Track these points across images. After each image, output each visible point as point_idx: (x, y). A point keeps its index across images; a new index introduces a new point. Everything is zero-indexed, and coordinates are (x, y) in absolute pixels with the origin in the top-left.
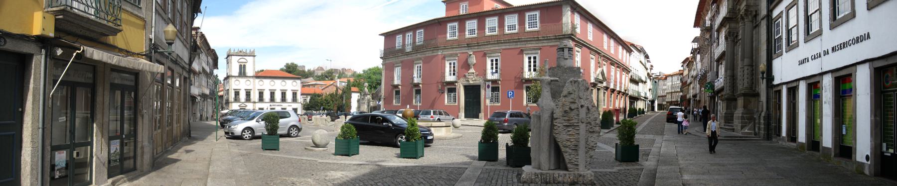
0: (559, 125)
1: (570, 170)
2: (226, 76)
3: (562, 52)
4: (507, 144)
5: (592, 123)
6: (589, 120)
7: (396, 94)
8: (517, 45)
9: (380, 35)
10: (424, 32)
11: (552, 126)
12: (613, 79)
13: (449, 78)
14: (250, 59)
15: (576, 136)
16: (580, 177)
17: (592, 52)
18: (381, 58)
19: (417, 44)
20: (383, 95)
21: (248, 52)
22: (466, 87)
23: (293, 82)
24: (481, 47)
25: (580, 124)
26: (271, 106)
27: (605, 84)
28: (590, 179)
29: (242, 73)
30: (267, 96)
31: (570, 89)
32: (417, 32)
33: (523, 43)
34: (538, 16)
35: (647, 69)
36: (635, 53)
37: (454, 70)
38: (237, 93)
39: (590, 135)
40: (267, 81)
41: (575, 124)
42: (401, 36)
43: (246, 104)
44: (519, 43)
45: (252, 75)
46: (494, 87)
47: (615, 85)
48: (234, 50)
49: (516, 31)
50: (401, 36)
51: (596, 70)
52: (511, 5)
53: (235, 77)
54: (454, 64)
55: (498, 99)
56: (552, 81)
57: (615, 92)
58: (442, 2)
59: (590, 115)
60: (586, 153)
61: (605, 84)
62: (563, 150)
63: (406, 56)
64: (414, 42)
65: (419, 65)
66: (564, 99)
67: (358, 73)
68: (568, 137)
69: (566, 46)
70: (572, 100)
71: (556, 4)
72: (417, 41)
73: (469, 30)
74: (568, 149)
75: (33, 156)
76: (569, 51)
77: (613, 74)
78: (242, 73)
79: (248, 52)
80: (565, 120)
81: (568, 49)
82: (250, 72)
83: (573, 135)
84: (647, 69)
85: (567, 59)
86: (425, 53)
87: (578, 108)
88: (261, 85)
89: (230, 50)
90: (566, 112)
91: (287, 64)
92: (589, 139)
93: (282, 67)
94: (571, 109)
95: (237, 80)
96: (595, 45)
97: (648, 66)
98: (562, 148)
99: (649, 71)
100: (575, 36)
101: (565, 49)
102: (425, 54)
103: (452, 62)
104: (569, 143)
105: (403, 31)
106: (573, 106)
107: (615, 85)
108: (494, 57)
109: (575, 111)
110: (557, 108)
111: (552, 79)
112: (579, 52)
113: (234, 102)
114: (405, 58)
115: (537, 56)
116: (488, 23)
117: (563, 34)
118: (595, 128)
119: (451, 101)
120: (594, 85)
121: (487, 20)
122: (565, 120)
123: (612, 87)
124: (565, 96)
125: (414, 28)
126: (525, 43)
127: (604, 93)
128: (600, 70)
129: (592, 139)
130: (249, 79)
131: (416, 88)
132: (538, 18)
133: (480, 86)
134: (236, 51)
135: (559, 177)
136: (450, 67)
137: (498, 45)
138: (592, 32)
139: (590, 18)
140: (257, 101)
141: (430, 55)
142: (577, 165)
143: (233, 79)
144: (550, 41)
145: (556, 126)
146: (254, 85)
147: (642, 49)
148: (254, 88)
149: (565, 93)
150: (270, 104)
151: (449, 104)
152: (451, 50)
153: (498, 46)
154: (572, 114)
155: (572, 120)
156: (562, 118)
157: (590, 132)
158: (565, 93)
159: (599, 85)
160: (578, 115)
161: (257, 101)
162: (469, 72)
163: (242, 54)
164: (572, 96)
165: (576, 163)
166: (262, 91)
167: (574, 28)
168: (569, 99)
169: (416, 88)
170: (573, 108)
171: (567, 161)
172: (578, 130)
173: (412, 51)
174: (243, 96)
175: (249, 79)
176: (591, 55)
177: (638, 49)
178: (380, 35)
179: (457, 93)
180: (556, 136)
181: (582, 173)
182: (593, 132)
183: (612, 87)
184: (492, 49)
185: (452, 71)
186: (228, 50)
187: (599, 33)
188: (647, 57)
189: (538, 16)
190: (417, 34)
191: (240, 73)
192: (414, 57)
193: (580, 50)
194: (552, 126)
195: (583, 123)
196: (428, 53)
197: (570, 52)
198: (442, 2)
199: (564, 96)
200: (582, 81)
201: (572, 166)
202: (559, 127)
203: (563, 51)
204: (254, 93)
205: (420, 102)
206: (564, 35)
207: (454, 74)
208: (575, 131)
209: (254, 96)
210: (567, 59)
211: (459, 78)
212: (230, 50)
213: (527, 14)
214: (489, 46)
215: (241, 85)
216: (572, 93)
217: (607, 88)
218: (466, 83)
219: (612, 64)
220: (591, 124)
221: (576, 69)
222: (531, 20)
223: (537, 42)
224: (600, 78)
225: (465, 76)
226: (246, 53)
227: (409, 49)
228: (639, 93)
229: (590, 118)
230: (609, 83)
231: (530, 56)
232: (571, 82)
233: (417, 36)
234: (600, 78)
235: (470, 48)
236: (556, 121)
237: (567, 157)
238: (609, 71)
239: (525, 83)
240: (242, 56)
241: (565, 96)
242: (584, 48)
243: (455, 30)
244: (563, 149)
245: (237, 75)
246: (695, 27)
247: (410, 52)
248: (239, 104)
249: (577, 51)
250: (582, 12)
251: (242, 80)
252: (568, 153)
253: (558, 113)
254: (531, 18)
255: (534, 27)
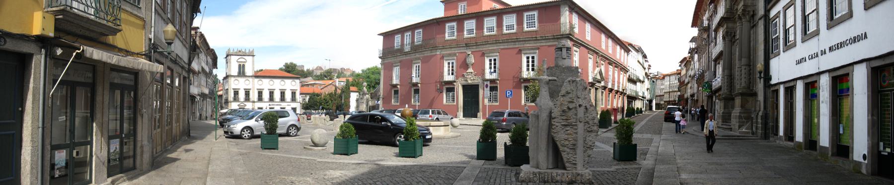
0: (557, 124)
1: (568, 169)
2: (225, 76)
3: (561, 52)
4: (505, 143)
5: (590, 122)
6: (587, 119)
7: (395, 94)
8: (515, 45)
9: (378, 35)
10: (423, 31)
11: (550, 125)
12: (611, 78)
13: (448, 77)
14: (249, 59)
15: (574, 135)
16: (578, 176)
17: (590, 52)
18: (380, 57)
19: (416, 44)
20: (382, 94)
21: (247, 51)
22: (464, 87)
23: (292, 82)
24: (480, 46)
25: (578, 123)
26: (270, 105)
27: (603, 84)
28: (588, 178)
29: (242, 73)
30: (266, 96)
31: (569, 89)
32: (416, 31)
33: (521, 43)
34: (536, 16)
35: (645, 69)
36: (633, 53)
37: (453, 70)
38: (236, 93)
39: (588, 134)
40: (266, 81)
41: (573, 124)
42: (400, 35)
43: (245, 103)
44: (517, 43)
45: (251, 75)
46: (492, 87)
47: (613, 85)
48: (233, 50)
49: (514, 31)
50: (400, 35)
51: (594, 69)
52: (509, 5)
53: (234, 76)
54: (453, 63)
55: (496, 98)
56: (550, 80)
57: (613, 92)
58: (441, 2)
59: (588, 114)
60: (584, 152)
61: (603, 84)
62: (561, 149)
63: (405, 56)
64: (413, 42)
65: (418, 65)
66: (562, 99)
67: (357, 72)
68: (566, 136)
69: (564, 45)
70: (570, 100)
71: (554, 4)
72: (416, 41)
73: (467, 30)
74: (566, 148)
75: (33, 155)
76: (567, 50)
77: (611, 73)
78: (242, 73)
79: (247, 51)
80: (563, 120)
81: (566, 49)
82: (249, 71)
83: (571, 134)
84: (645, 69)
85: (565, 59)
86: (424, 52)
87: (576, 108)
88: (260, 85)
89: (229, 50)
90: (564, 111)
91: (286, 64)
92: (587, 138)
93: (281, 67)
94: (569, 109)
95: (236, 80)
96: (593, 45)
97: (646, 65)
98: (560, 147)
99: (647, 70)
100: (573, 36)
101: (563, 49)
102: (424, 54)
103: (451, 62)
104: (567, 143)
105: (402, 31)
106: (571, 106)
107: (613, 85)
108: (492, 56)
109: (573, 110)
110: (556, 107)
111: (550, 78)
112: (577, 52)
113: (233, 102)
114: (404, 58)
115: (535, 56)
116: (487, 23)
117: (561, 33)
118: (593, 127)
119: (449, 101)
120: (592, 85)
121: (486, 19)
122: (563, 120)
123: (610, 86)
124: (563, 96)
125: (412, 28)
126: (524, 43)
127: (602, 92)
128: (598, 69)
129: (590, 138)
130: (248, 79)
131: (415, 88)
132: (536, 18)
133: (478, 85)
134: (235, 51)
135: (557, 176)
136: (449, 67)
137: (496, 45)
138: (590, 32)
139: (588, 18)
140: (256, 101)
141: (428, 55)
142: (575, 164)
143: (233, 79)
144: (548, 41)
145: (554, 125)
146: (253, 84)
147: (640, 48)
148: (254, 87)
149: (563, 92)
150: (269, 103)
151: (447, 104)
152: (450, 49)
153: (497, 46)
154: (570, 113)
155: (570, 119)
156: (560, 117)
157: (588, 131)
158: (563, 92)
159: (597, 84)
160: (576, 115)
161: (256, 100)
162: (467, 71)
163: (241, 54)
164: (570, 95)
165: (574, 162)
166: (262, 90)
167: (572, 27)
168: (567, 99)
169: (415, 88)
170: (571, 107)
171: (565, 160)
172: (576, 129)
173: (411, 51)
174: (242, 96)
175: (248, 79)
176: (589, 55)
177: (636, 49)
178: (378, 35)
179: (455, 93)
180: (555, 135)
181: (580, 172)
182: (591, 131)
183: (610, 86)
184: (490, 48)
185: (451, 70)
186: (227, 50)
187: (597, 33)
188: (645, 56)
189: (536, 16)
190: (416, 34)
191: (239, 73)
192: (413, 56)
193: (578, 50)
194: (550, 125)
195: (581, 122)
196: (426, 52)
197: (568, 52)
198: (441, 2)
199: (562, 96)
200: (580, 81)
201: (570, 165)
202: (557, 126)
203: (561, 51)
204: (253, 92)
205: (418, 102)
206: (562, 35)
207: (452, 74)
208: (573, 130)
209: (253, 96)
210: (565, 59)
211: (457, 77)
212: (229, 50)
213: (525, 14)
214: (487, 46)
215: (240, 84)
216: (570, 93)
217: (605, 88)
218: (464, 83)
219: (610, 64)
220: (589, 124)
221: (574, 68)
222: (529, 20)
223: (535, 42)
224: (598, 77)
225: (463, 76)
226: (246, 53)
227: (407, 48)
228: (636, 92)
229: (588, 117)
230: (607, 82)
231: (528, 55)
232: (569, 81)
233: (416, 35)
234: (598, 77)
235: (468, 48)
236: (554, 120)
237: (565, 156)
238: (607, 71)
239: (523, 83)
240: (241, 55)
241: (563, 96)
242: (582, 48)
243: (454, 29)
244: (561, 148)
245: (237, 75)
246: (692, 26)
247: (409, 51)
248: (238, 103)
249: (575, 51)
250: (580, 12)
251: (242, 80)
252: (566, 152)
253: (556, 112)
254: (529, 18)
255: (532, 27)
